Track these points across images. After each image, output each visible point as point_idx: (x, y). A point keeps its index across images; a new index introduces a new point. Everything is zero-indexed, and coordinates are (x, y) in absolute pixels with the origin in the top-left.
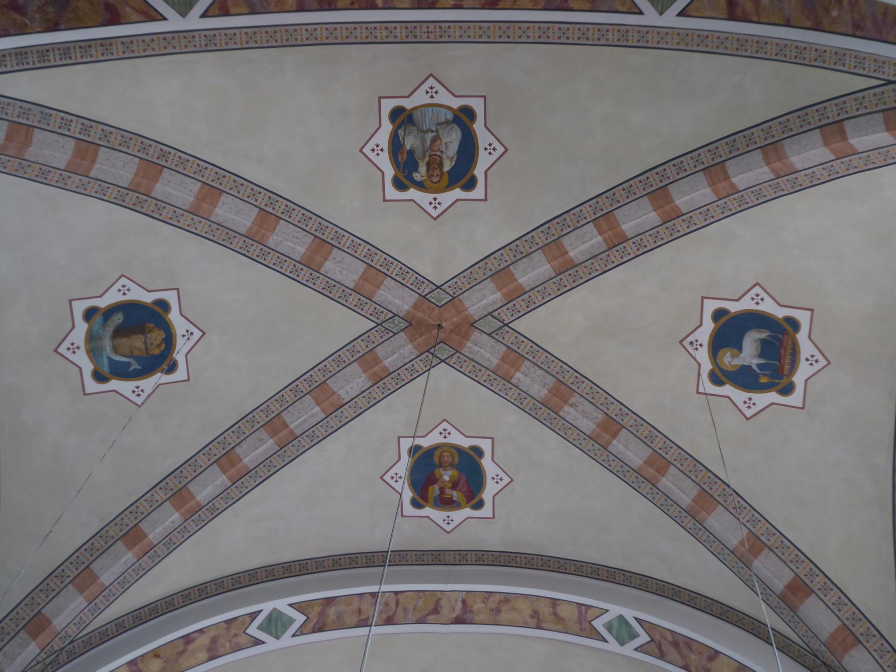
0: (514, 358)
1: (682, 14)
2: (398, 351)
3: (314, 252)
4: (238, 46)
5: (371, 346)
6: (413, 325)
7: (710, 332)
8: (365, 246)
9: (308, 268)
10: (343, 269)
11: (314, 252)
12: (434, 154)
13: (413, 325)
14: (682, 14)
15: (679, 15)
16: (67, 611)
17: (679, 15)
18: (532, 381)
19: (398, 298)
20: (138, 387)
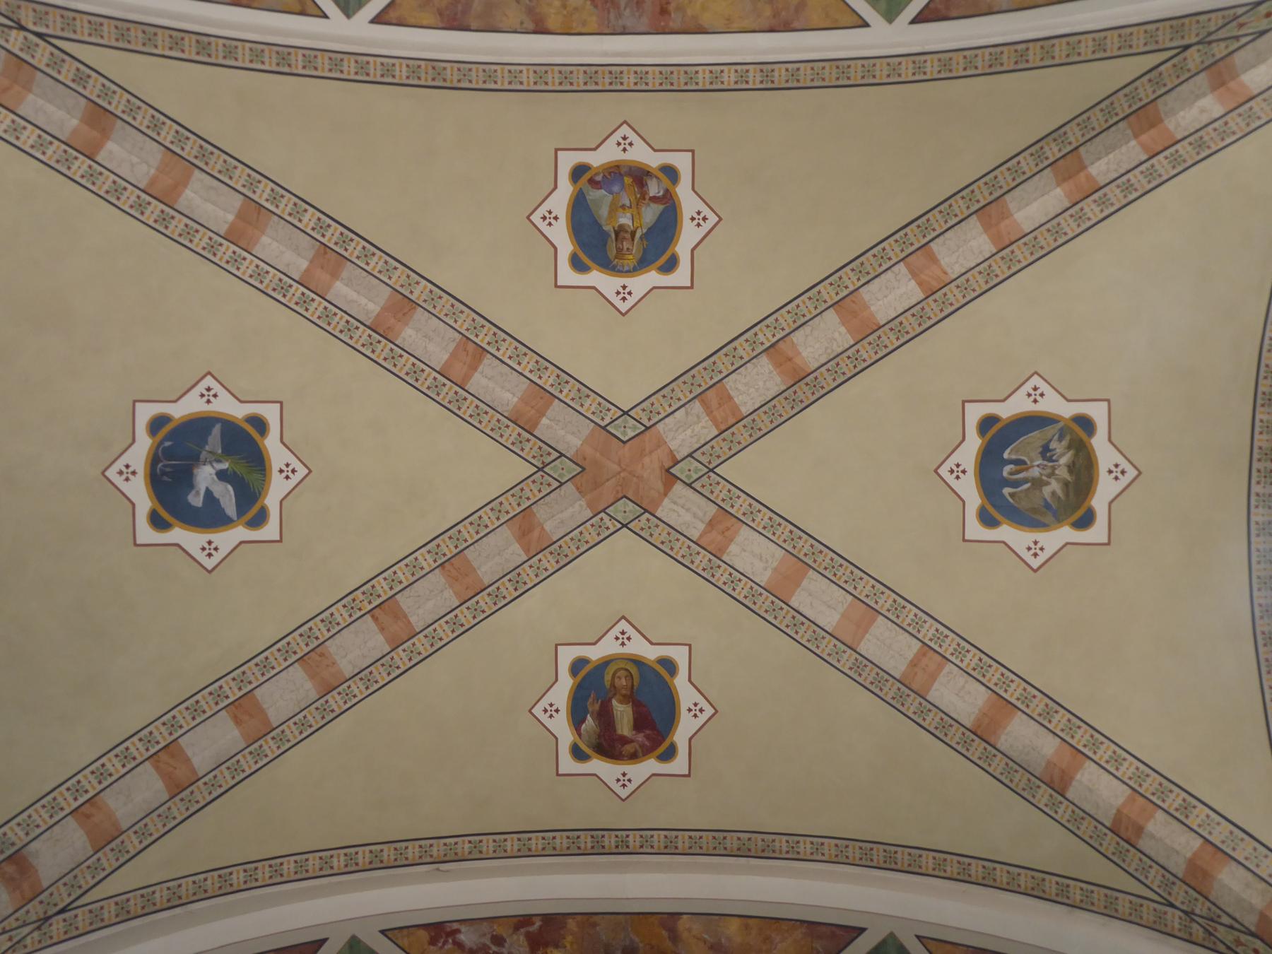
0: (725, 520)
1: (377, 20)
2: (563, 513)
3: (465, 363)
4: (1024, 263)
5: (526, 504)
6: (586, 474)
7: (1098, 454)
8: (306, 226)
9: (450, 385)
10: (498, 386)
11: (465, 363)
12: (623, 223)
13: (586, 474)
14: (377, 20)
15: (373, 21)
16: (50, 108)
17: (373, 21)
18: (498, 386)
19: (565, 430)
20: (208, 402)
